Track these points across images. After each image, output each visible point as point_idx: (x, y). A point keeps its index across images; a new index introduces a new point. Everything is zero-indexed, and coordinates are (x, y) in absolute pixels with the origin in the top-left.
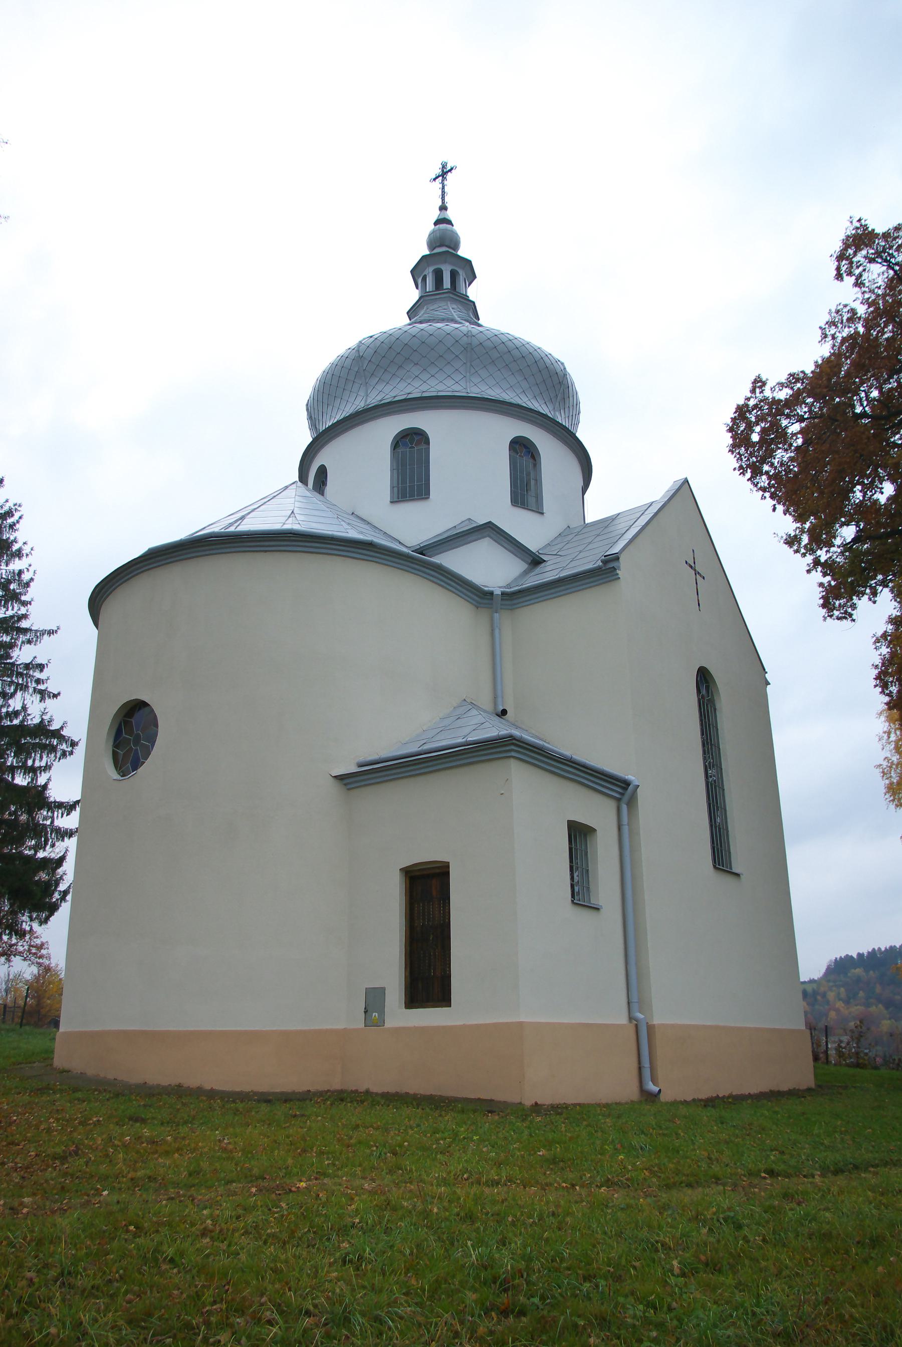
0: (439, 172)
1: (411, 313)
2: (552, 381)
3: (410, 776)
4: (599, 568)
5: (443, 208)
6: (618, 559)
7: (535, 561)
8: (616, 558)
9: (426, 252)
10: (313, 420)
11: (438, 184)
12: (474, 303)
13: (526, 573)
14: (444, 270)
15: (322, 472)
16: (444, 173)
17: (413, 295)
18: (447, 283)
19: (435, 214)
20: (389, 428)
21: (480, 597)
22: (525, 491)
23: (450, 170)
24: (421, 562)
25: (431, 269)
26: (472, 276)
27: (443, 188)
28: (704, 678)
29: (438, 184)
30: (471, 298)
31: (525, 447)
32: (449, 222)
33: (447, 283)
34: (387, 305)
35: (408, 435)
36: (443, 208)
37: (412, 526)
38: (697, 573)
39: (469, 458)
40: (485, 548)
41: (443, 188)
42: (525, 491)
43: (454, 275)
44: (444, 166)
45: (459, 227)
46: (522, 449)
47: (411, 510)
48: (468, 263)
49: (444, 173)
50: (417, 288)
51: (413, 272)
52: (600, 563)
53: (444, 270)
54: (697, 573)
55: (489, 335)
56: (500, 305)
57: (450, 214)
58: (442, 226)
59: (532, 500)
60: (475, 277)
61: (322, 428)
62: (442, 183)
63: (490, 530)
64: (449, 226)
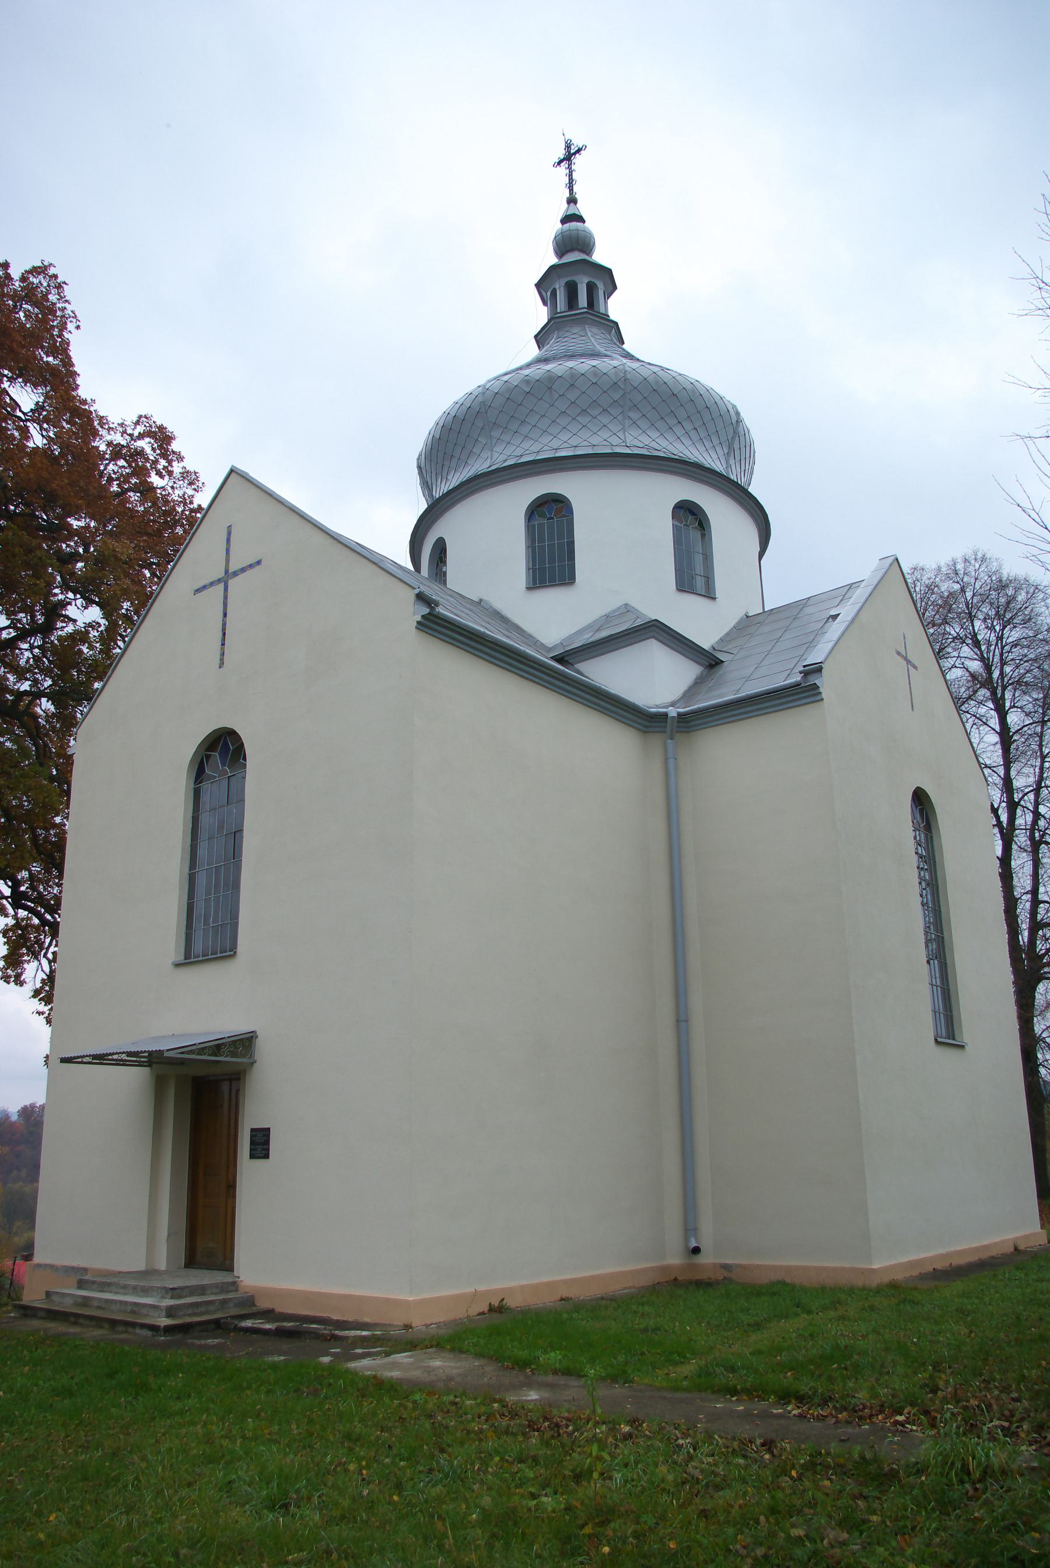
0: (561, 153)
1: (540, 339)
2: (721, 424)
3: (497, 645)
4: (797, 685)
5: (572, 200)
6: (819, 670)
7: (710, 662)
8: (817, 669)
9: (554, 260)
10: (426, 486)
11: (563, 170)
12: (616, 324)
13: (698, 682)
14: (576, 285)
15: (440, 551)
16: (569, 156)
17: (541, 315)
18: (583, 300)
19: (562, 208)
20: (513, 502)
21: (646, 721)
22: (694, 575)
23: (579, 151)
24: (559, 673)
25: (563, 281)
26: (612, 287)
27: (570, 175)
28: (920, 799)
29: (563, 170)
30: (612, 317)
31: (693, 514)
32: (580, 219)
33: (583, 300)
34: (504, 334)
35: (546, 502)
36: (572, 200)
37: (551, 620)
38: (908, 662)
39: (622, 526)
40: (654, 655)
41: (570, 175)
42: (694, 575)
43: (591, 288)
44: (568, 146)
45: (593, 224)
46: (689, 515)
47: (552, 597)
48: (607, 274)
49: (569, 156)
50: (545, 303)
51: (538, 285)
52: (798, 678)
53: (576, 285)
54: (908, 662)
55: (645, 372)
56: (653, 325)
57: (583, 208)
58: (574, 225)
59: (700, 582)
60: (615, 288)
61: (437, 495)
62: (569, 168)
63: (656, 630)
64: (580, 224)
